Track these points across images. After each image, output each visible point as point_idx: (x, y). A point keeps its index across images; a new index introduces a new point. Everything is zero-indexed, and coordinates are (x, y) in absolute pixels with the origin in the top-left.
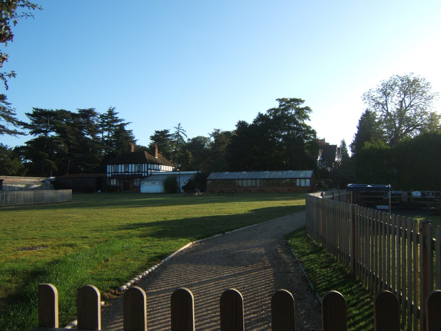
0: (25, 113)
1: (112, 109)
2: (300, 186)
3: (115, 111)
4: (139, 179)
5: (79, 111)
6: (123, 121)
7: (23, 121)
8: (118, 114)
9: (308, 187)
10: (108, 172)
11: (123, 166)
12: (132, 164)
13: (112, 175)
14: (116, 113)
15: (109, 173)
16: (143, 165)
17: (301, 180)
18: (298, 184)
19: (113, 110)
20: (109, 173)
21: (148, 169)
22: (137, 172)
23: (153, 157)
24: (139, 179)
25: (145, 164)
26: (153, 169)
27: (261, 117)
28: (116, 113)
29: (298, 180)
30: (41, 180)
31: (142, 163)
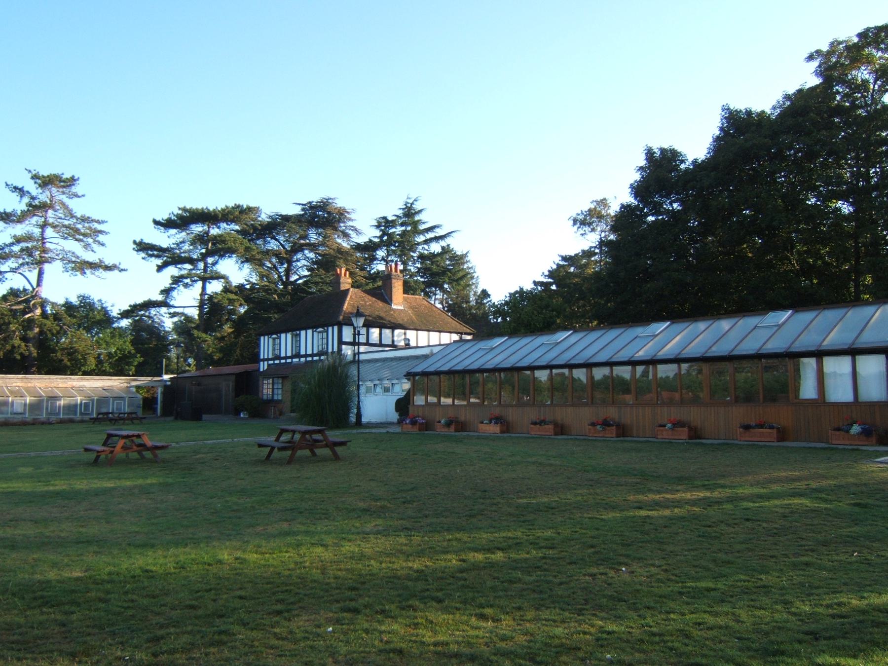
0: (156, 223)
1: (411, 201)
2: (821, 402)
3: (417, 206)
4: (271, 381)
5: (303, 210)
6: (437, 230)
7: (146, 241)
8: (423, 213)
9: (872, 405)
10: (262, 357)
11: (289, 335)
12: (306, 329)
13: (269, 365)
14: (420, 211)
15: (264, 360)
16: (330, 329)
17: (861, 360)
18: (808, 390)
19: (412, 204)
20: (264, 360)
21: (341, 342)
22: (316, 355)
23: (380, 304)
24: (271, 381)
25: (332, 326)
26: (368, 344)
27: (739, 128)
28: (420, 211)
29: (809, 365)
30: (134, 383)
31: (328, 326)
